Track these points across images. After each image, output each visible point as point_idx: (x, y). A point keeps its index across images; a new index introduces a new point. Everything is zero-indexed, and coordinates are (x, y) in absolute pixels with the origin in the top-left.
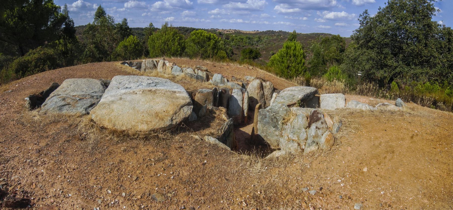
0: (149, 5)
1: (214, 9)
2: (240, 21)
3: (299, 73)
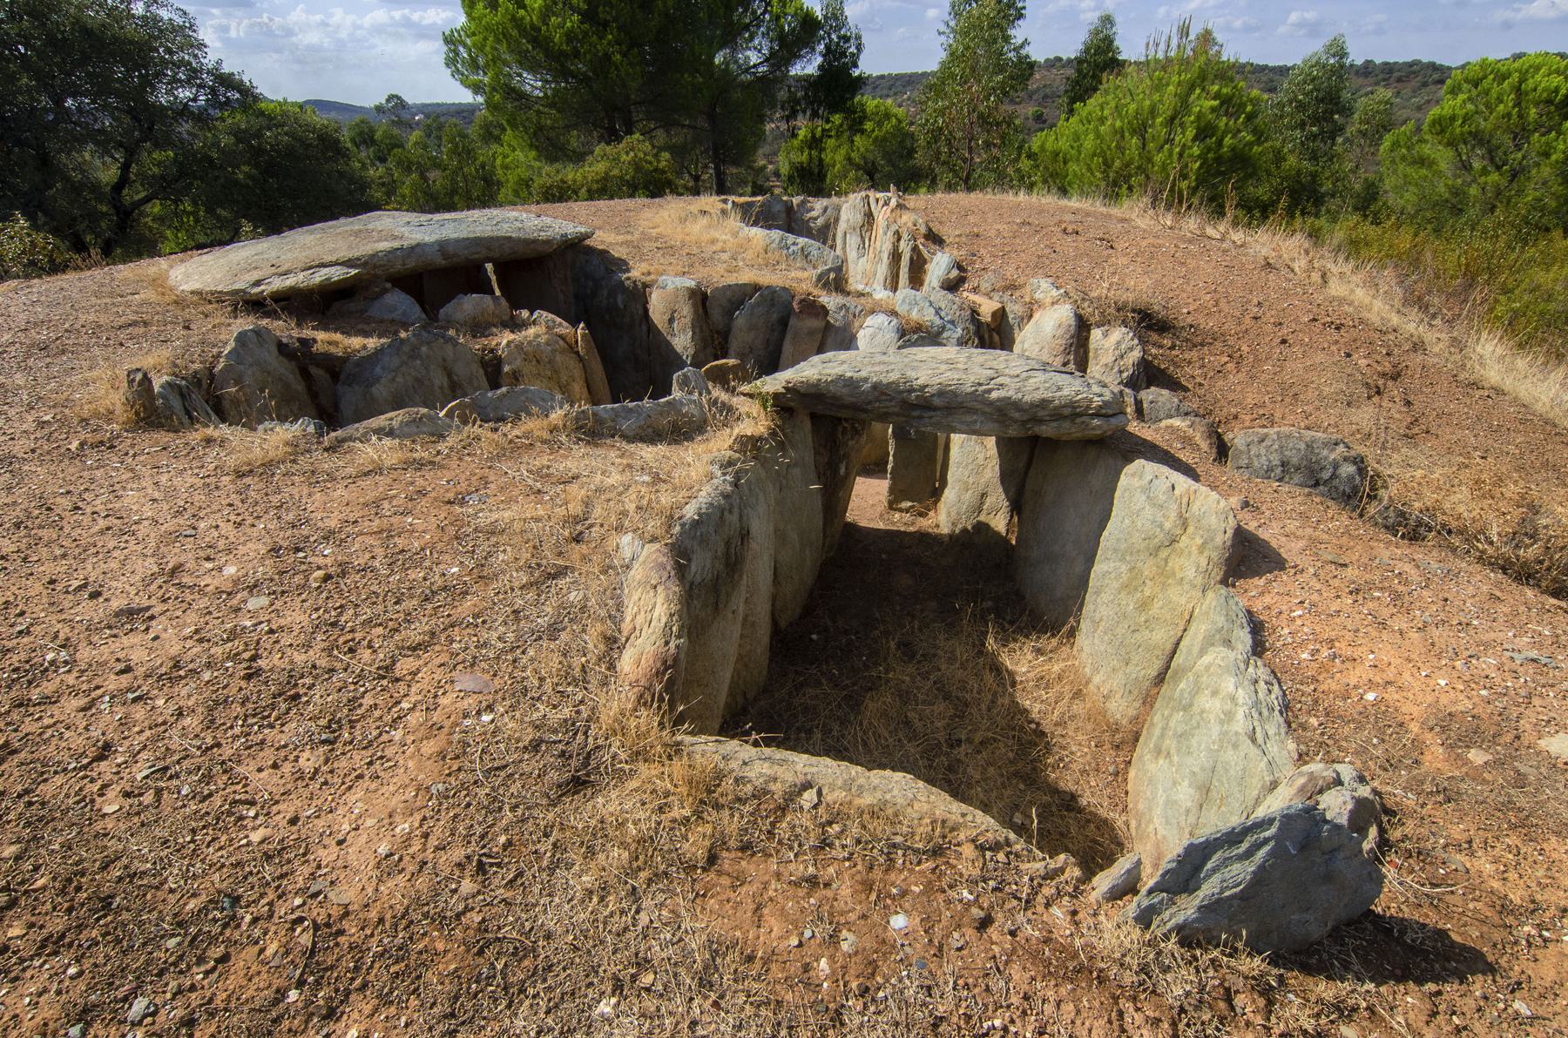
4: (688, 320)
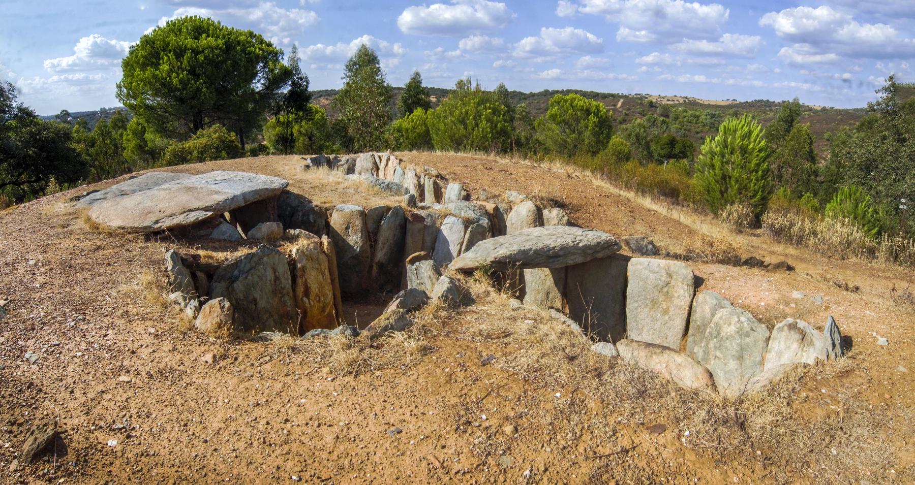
0: (509, 45)
1: (647, 55)
2: (700, 78)
3: (750, 194)
4: (359, 228)
